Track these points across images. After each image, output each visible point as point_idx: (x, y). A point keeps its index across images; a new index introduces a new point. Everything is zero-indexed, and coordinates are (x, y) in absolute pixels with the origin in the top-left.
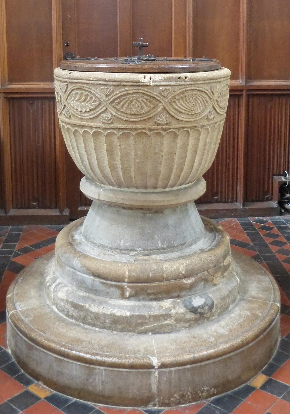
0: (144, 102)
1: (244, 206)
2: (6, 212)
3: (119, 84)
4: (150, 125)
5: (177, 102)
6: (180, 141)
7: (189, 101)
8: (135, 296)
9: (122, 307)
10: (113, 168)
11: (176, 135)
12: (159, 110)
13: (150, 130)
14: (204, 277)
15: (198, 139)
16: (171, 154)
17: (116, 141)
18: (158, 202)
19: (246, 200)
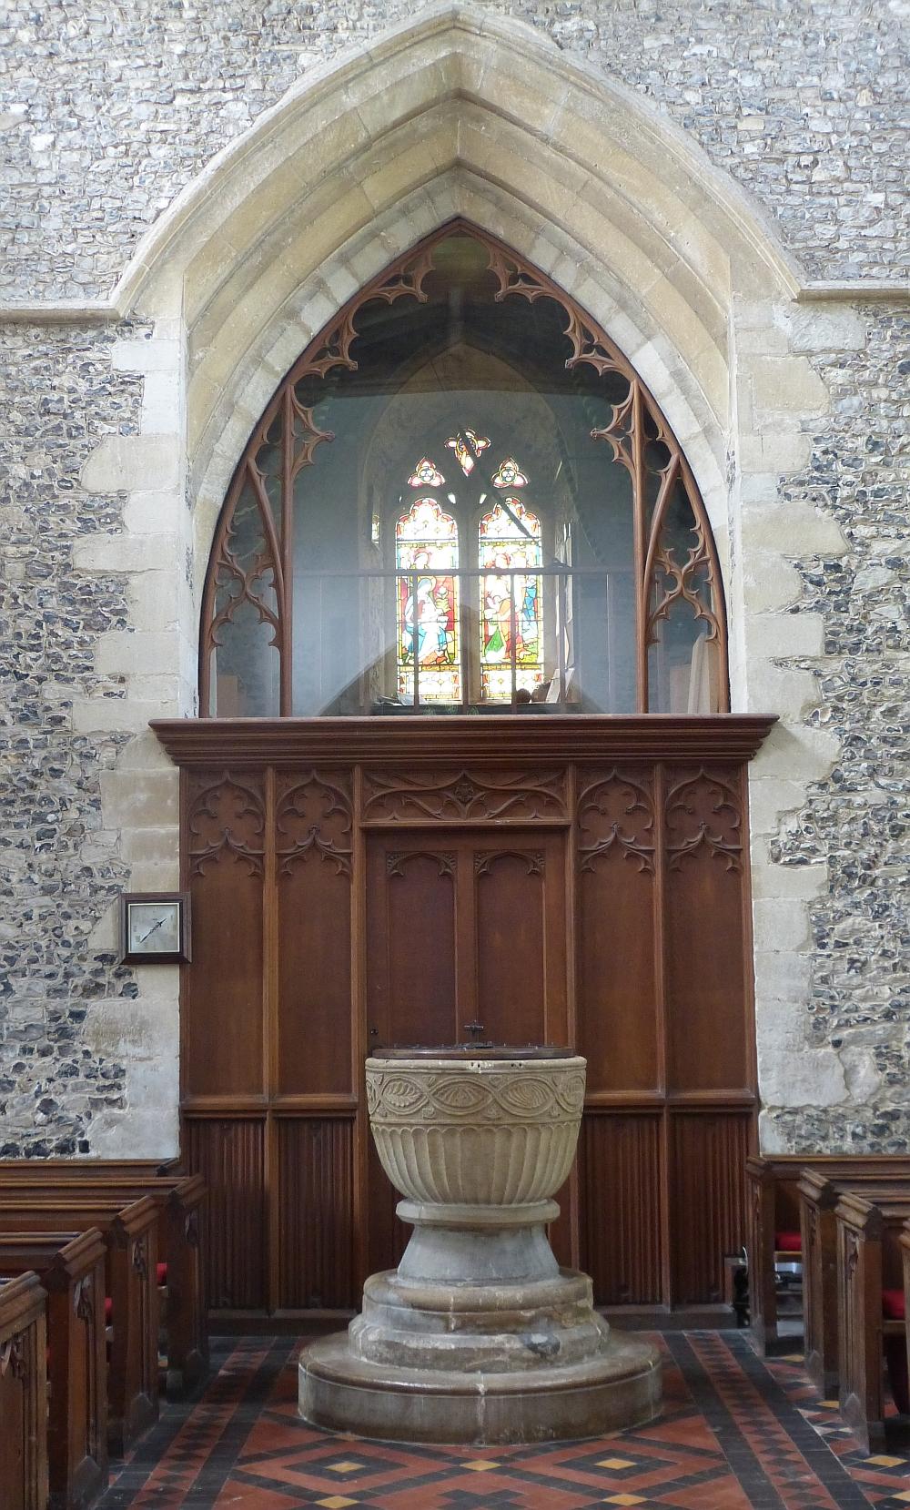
1: (673, 1309)
2: (269, 1312)
3: (444, 1072)
4: (479, 1119)
6: (515, 1141)
8: (461, 1328)
9: (446, 1342)
10: (437, 1174)
11: (510, 1134)
13: (479, 1125)
14: (550, 1312)
15: (538, 1140)
16: (505, 1156)
17: (440, 1140)
19: (676, 1302)
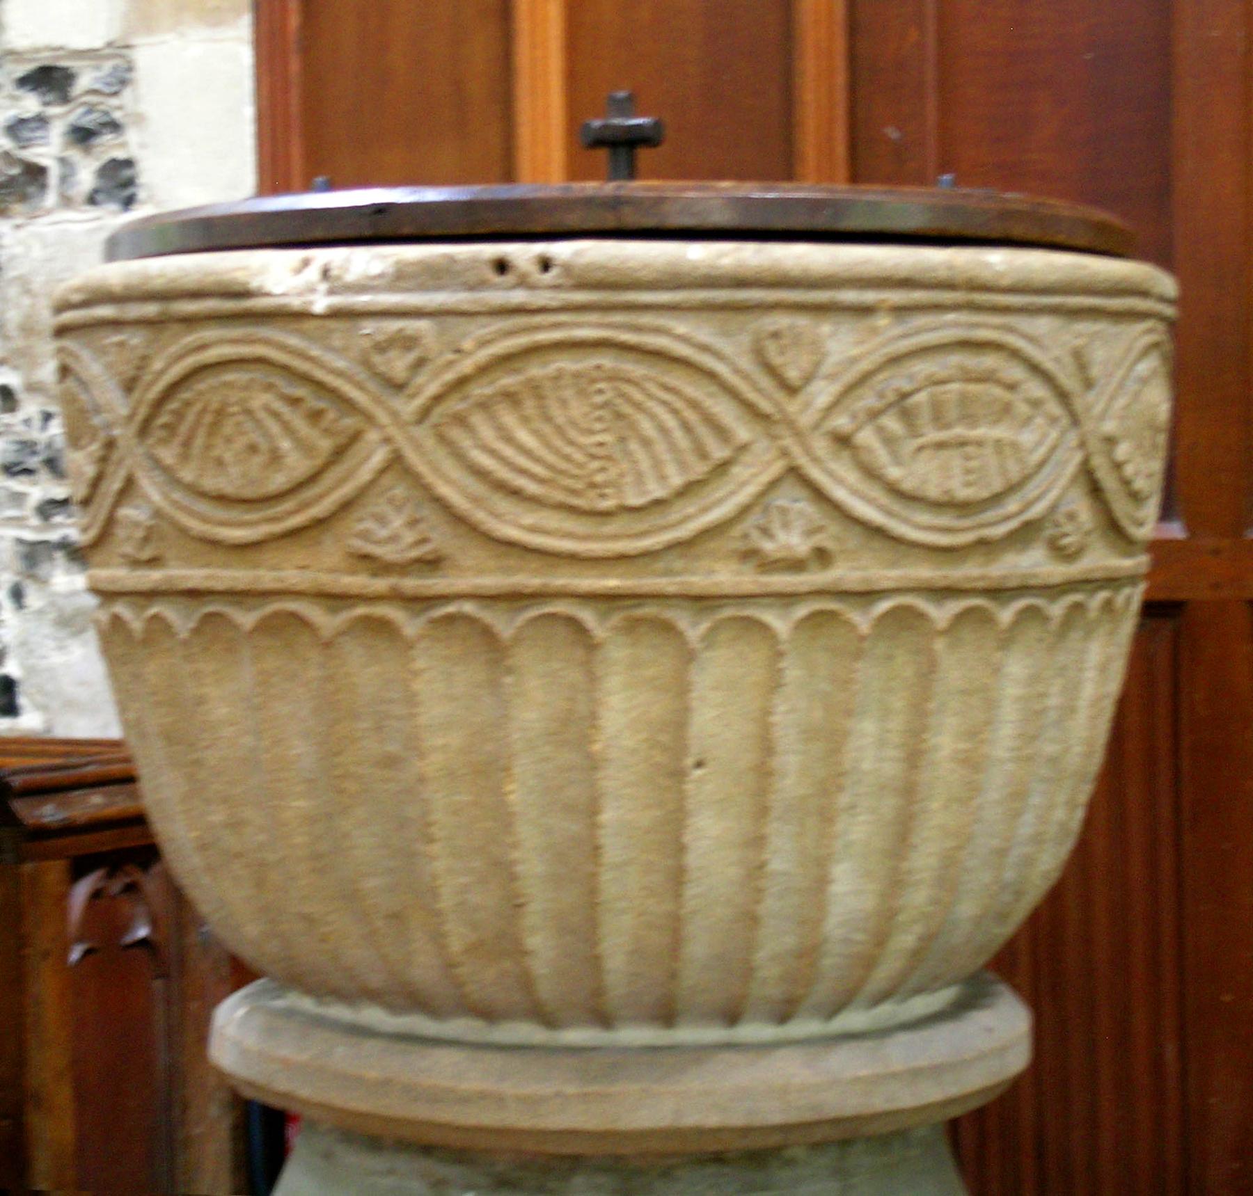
0: (276, 415)
5: (477, 419)
7: (560, 420)
12: (365, 474)
13: (335, 599)
18: (465, 1100)
